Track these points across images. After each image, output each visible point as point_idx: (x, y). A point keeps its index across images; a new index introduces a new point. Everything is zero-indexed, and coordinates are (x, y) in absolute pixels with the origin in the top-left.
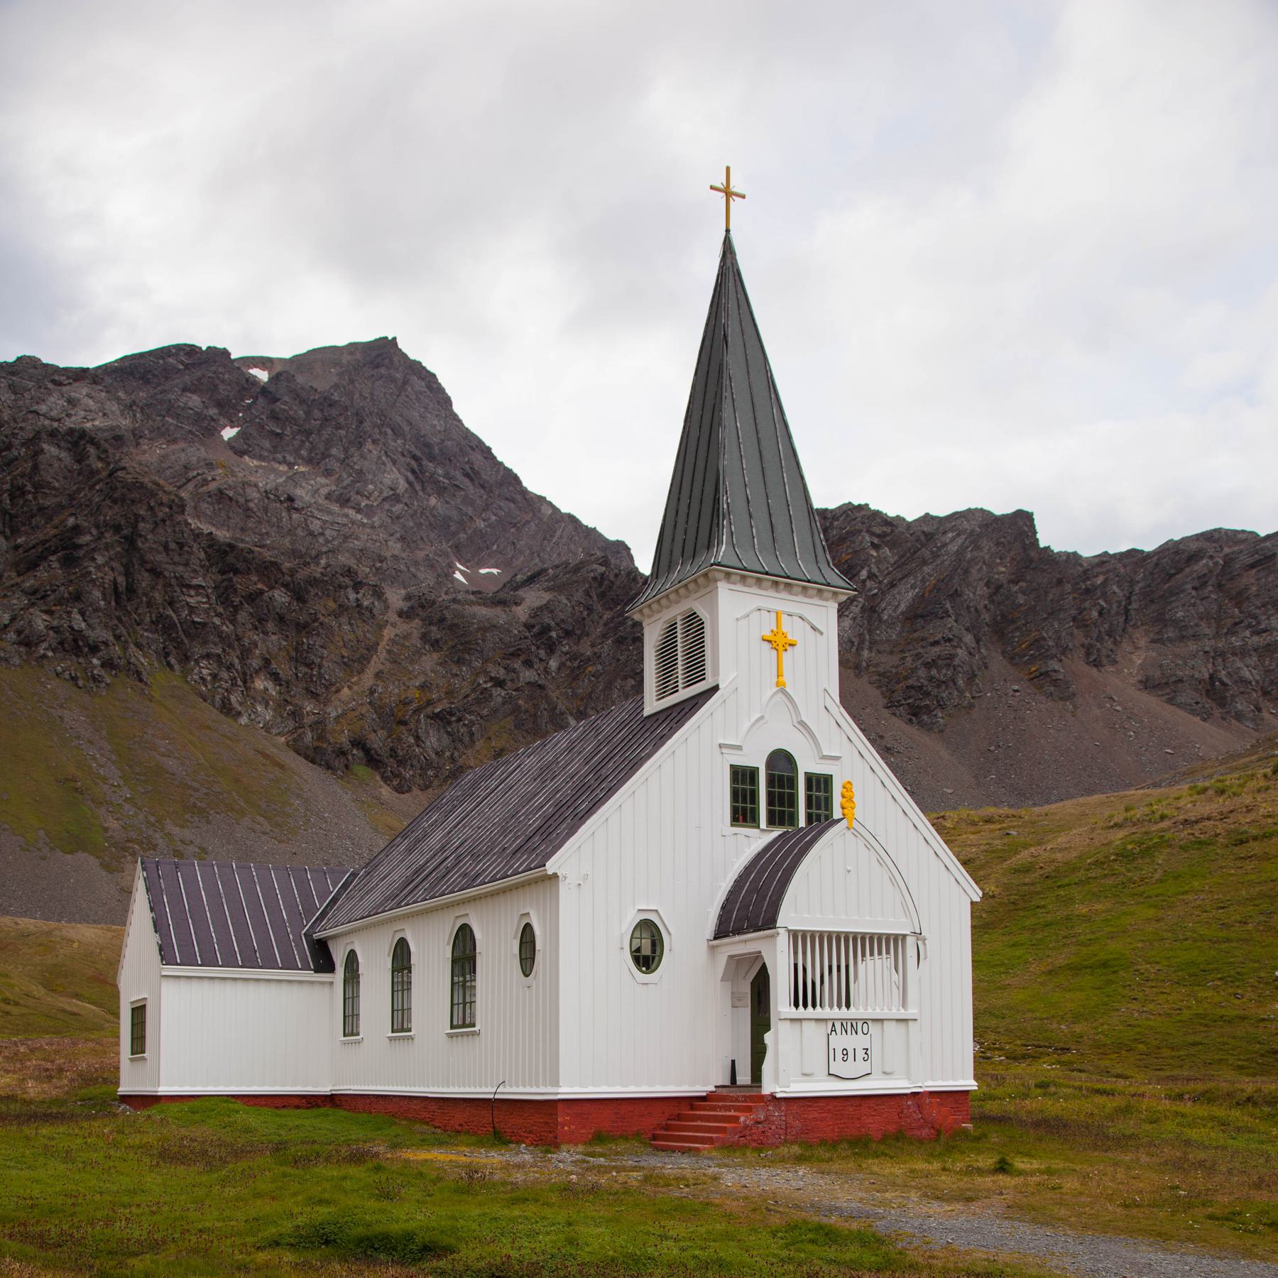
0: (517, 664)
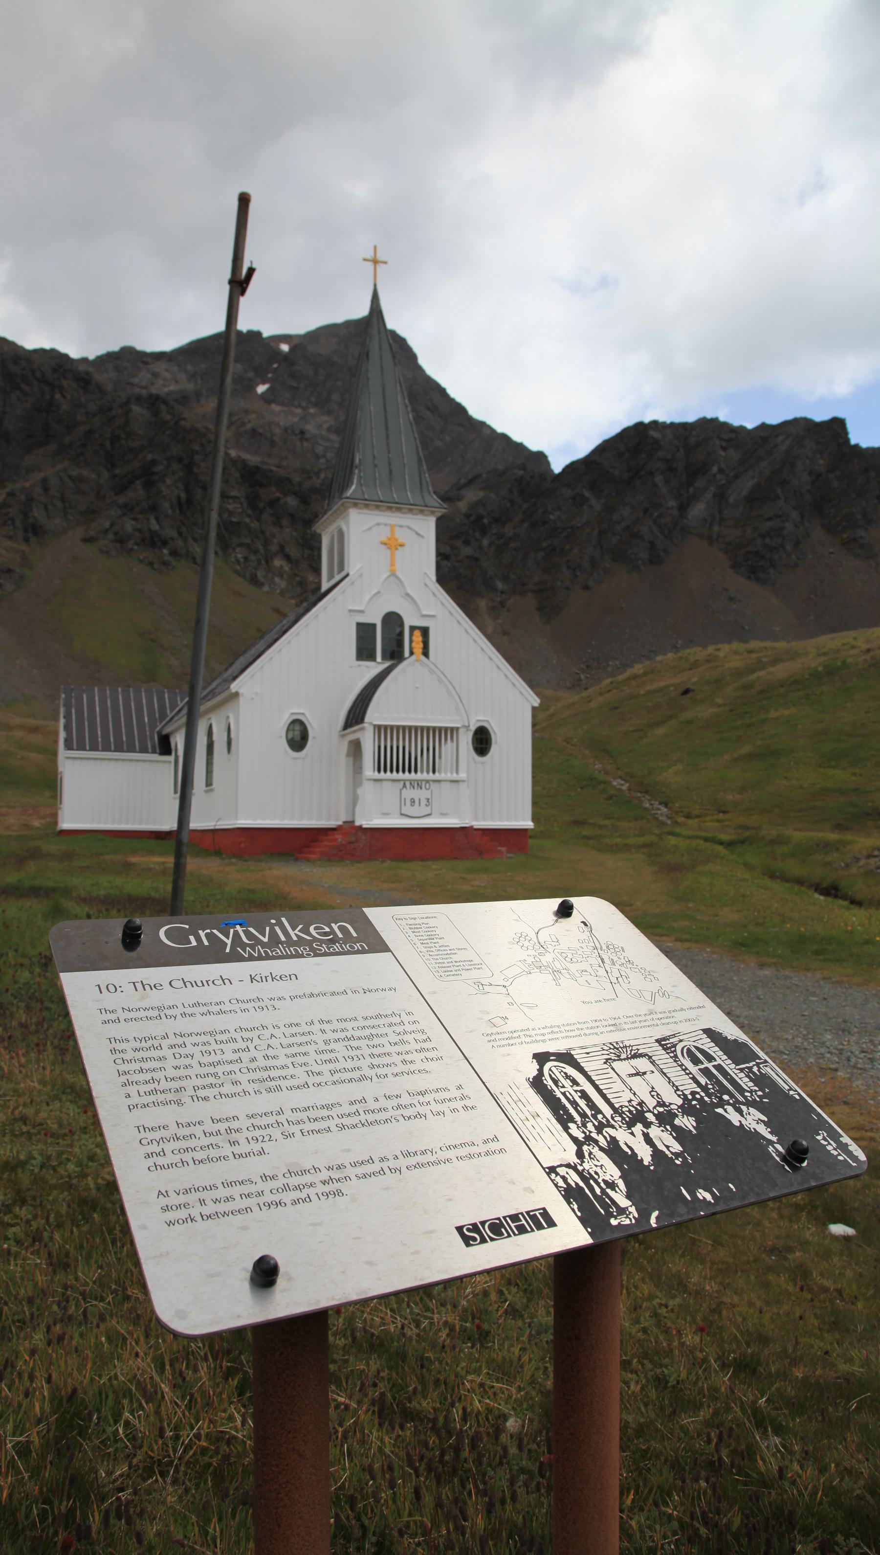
0: (459, 543)
